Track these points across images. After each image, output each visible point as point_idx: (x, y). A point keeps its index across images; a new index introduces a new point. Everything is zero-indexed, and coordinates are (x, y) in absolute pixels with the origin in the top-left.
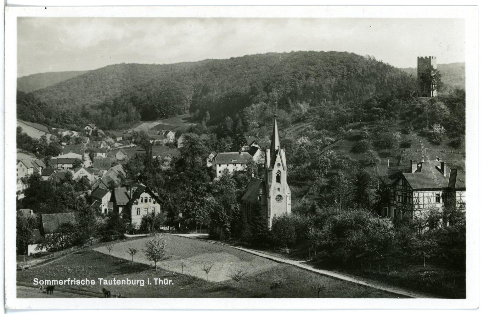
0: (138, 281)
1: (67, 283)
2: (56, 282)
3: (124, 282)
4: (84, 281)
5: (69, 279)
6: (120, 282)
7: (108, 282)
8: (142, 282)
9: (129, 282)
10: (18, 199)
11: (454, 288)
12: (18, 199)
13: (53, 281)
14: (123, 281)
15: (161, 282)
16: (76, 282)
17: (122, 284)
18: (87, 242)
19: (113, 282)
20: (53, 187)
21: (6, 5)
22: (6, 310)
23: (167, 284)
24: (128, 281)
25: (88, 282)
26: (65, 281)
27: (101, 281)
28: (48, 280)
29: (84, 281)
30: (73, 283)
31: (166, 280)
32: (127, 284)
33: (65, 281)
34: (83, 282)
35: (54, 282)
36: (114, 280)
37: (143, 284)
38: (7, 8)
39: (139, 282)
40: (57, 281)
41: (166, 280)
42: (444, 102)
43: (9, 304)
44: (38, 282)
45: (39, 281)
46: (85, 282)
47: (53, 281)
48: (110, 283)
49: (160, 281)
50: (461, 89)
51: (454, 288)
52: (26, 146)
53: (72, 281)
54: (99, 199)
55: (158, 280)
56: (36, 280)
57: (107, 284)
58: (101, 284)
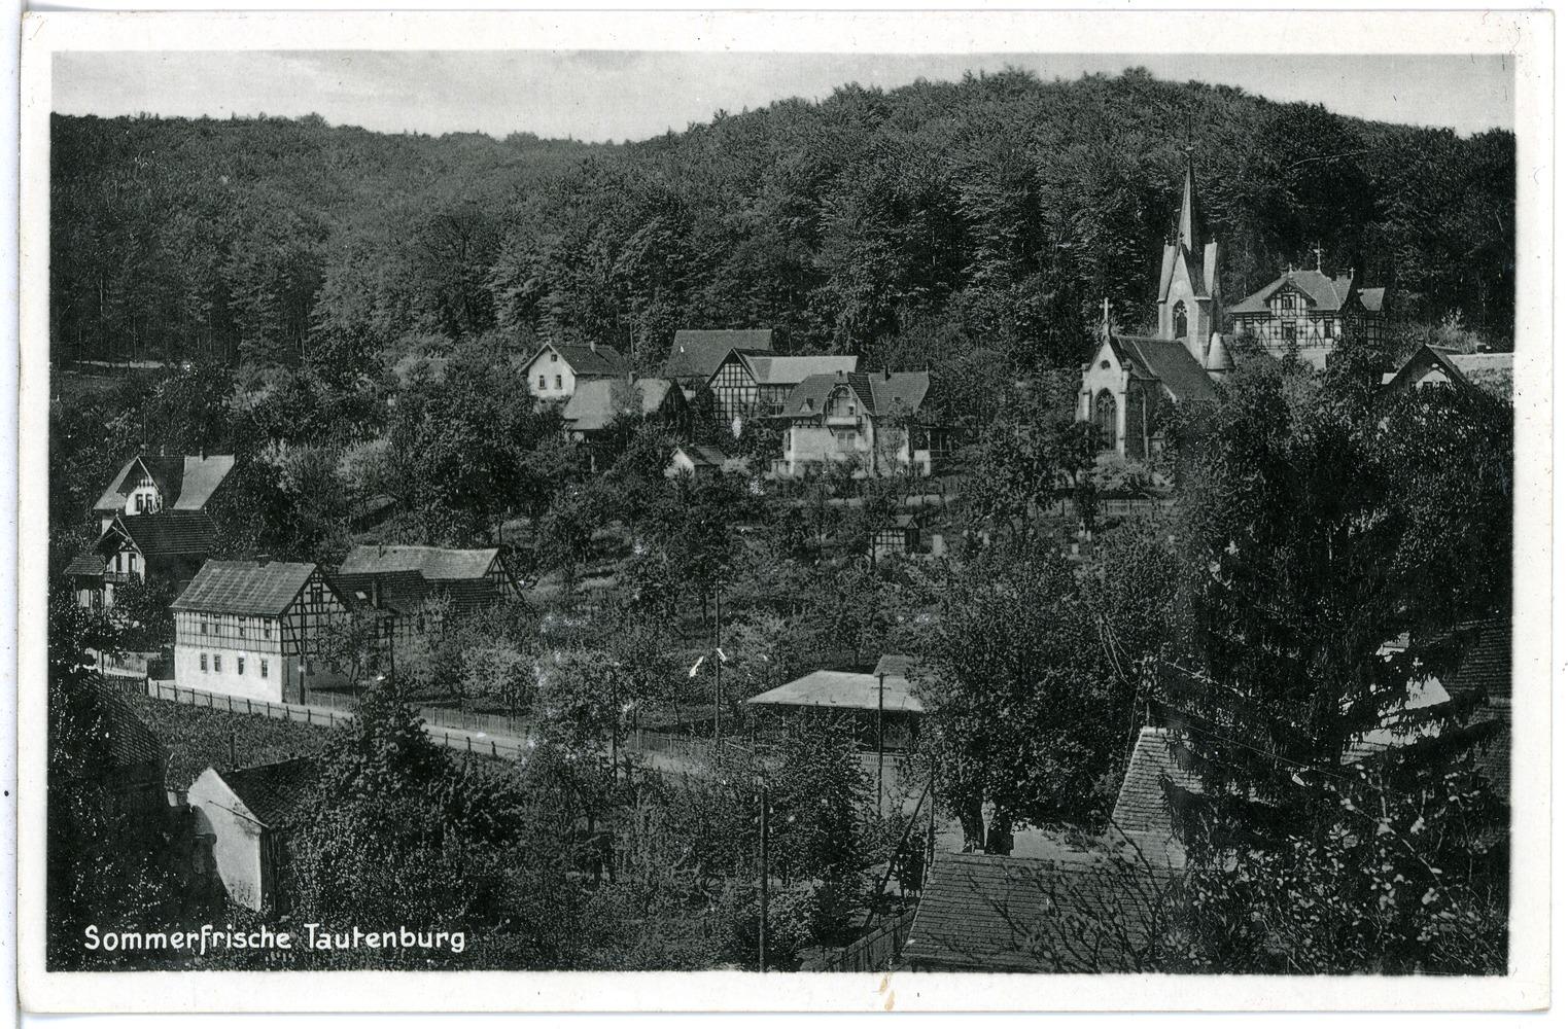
2: (136, 939)
3: (341, 942)
7: (333, 939)
13: (149, 937)
15: (268, 940)
17: (124, 947)
20: (539, 470)
21: (26, 8)
24: (404, 935)
25: (268, 940)
28: (157, 933)
35: (128, 940)
37: (462, 945)
38: (32, 22)
40: (164, 936)
42: (561, 402)
43: (30, 1000)
44: (244, 940)
45: (101, 936)
47: (124, 937)
52: (256, 401)
54: (1362, 279)
56: (92, 932)
57: (328, 945)
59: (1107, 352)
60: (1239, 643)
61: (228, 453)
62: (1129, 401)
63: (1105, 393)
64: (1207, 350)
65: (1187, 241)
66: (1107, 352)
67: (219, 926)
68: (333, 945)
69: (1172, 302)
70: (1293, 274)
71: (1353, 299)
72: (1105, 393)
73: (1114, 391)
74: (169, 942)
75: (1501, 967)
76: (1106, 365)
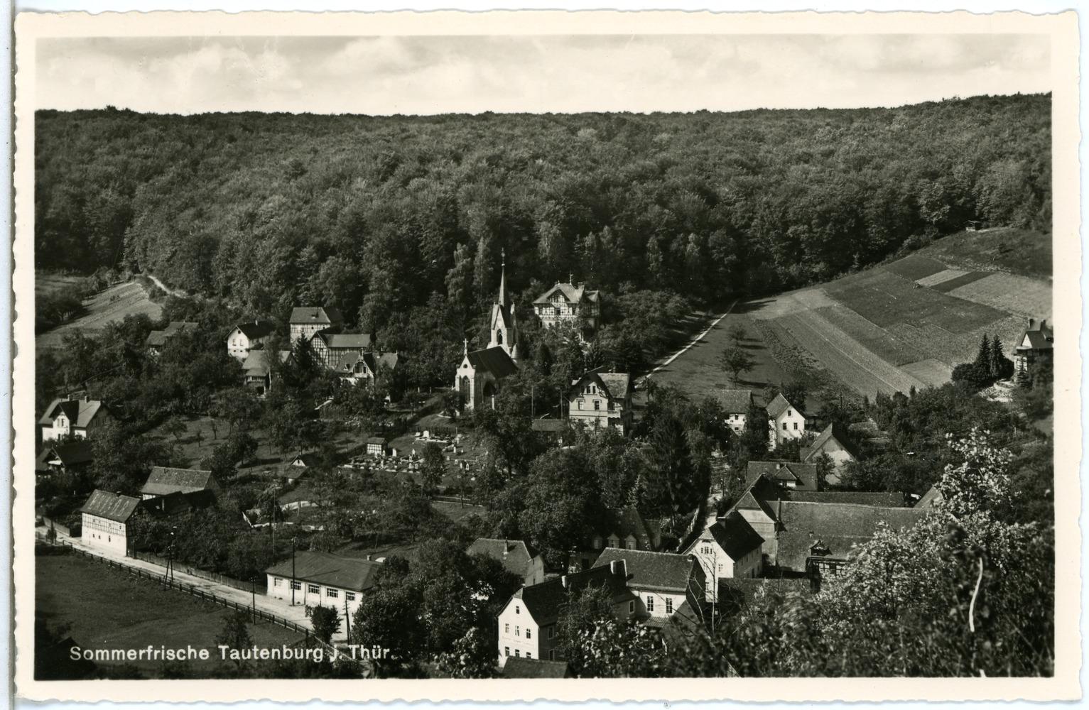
0: (308, 651)
1: (145, 655)
4: (184, 651)
5: (150, 647)
6: (135, 653)
8: (318, 654)
9: (288, 653)
10: (291, 561)
11: (1029, 651)
12: (291, 561)
13: (113, 652)
14: (274, 651)
15: (193, 653)
16: (166, 655)
17: (273, 657)
18: (444, 573)
19: (252, 652)
22: (13, 702)
23: (302, 657)
24: (285, 651)
26: (141, 652)
27: (354, 652)
29: (184, 651)
30: (159, 655)
31: (377, 649)
32: (285, 657)
33: (141, 652)
34: (182, 655)
36: (255, 649)
37: (321, 657)
39: (311, 654)
41: (377, 649)
46: (186, 655)
48: (246, 655)
49: (363, 650)
50: (42, 271)
51: (1029, 651)
53: (156, 652)
55: (358, 650)
57: (238, 657)
58: (224, 657)
59: (466, 361)
60: (422, 613)
61: (97, 400)
62: (475, 382)
63: (466, 377)
64: (511, 350)
65: (502, 303)
66: (466, 361)
67: (157, 647)
68: (241, 656)
69: (497, 329)
70: (559, 285)
71: (585, 296)
72: (466, 377)
73: (469, 377)
74: (166, 655)
75: (1047, 673)
76: (466, 366)
